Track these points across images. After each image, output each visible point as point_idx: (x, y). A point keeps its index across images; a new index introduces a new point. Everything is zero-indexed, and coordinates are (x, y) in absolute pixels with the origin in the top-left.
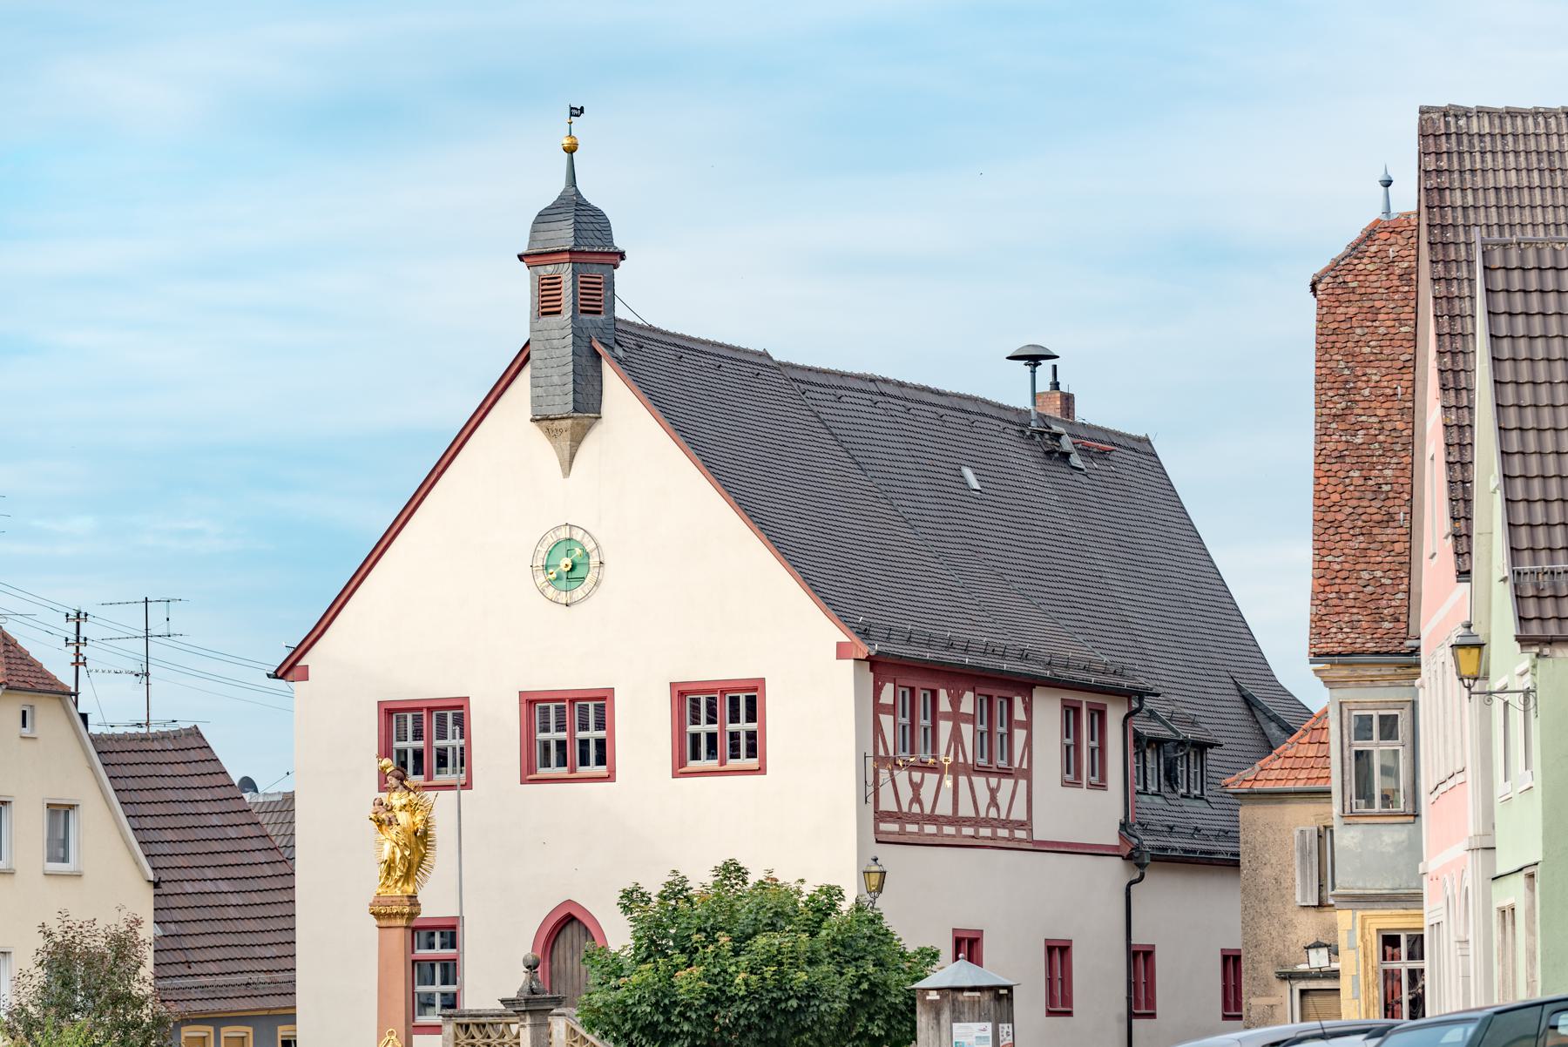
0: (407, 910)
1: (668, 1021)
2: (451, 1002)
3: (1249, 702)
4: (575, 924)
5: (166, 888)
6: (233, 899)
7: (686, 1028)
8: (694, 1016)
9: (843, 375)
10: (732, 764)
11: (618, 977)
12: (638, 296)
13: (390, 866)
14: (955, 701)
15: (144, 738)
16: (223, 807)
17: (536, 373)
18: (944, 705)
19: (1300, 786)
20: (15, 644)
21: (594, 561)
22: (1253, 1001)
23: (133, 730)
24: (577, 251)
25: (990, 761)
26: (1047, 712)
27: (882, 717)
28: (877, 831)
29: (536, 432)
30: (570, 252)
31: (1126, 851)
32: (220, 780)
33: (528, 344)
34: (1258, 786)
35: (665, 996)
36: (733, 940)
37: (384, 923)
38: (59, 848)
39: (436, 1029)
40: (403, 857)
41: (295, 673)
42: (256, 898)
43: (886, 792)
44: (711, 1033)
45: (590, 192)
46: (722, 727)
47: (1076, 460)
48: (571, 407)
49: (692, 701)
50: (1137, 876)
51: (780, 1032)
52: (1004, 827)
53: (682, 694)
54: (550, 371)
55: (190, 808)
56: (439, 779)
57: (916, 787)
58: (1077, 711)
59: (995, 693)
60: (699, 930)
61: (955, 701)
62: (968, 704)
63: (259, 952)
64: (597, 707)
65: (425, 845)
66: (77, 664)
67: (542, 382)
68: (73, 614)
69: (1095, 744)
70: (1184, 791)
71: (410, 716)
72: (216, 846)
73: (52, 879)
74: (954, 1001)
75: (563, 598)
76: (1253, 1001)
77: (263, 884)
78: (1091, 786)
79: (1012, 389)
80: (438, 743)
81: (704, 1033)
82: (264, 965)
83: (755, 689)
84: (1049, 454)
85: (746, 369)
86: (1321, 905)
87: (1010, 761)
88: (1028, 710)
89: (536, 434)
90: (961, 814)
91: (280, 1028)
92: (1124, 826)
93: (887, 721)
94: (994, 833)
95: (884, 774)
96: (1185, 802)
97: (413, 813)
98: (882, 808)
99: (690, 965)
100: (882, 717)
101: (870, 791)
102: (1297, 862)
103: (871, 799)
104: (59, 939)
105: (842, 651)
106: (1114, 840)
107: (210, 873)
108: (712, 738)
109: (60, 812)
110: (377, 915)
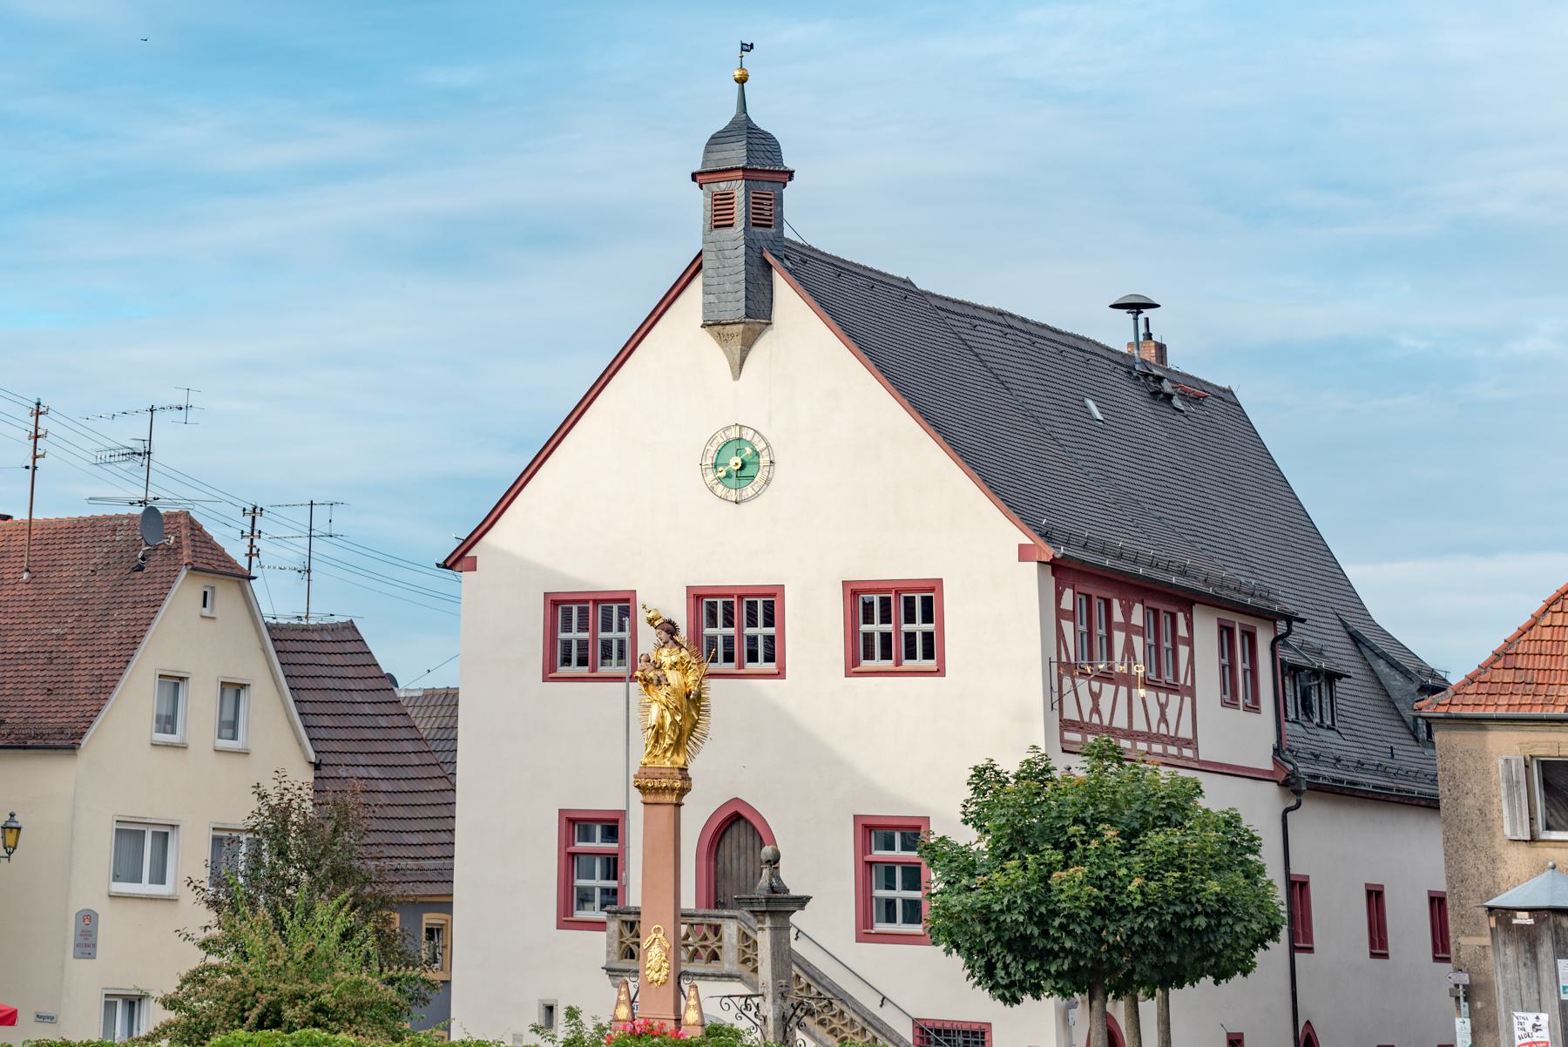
0: (678, 784)
1: (1045, 934)
2: (611, 896)
3: (1356, 639)
4: (742, 823)
5: (325, 772)
6: (384, 786)
7: (1068, 944)
8: (1079, 931)
9: (976, 307)
10: (908, 664)
11: (972, 876)
12: (804, 219)
13: (658, 733)
14: (1127, 613)
15: (305, 629)
16: (375, 697)
17: (709, 281)
18: (1118, 616)
19: (1502, 712)
20: (200, 529)
21: (764, 460)
22: (1463, 940)
23: (295, 622)
24: (750, 169)
25: (1159, 675)
26: (1206, 630)
27: (1063, 622)
28: (1062, 741)
29: (706, 338)
30: (744, 169)
31: (1282, 777)
32: (372, 671)
33: (700, 254)
34: (1454, 711)
35: (1040, 902)
36: (1121, 834)
37: (651, 799)
38: (230, 727)
39: (600, 926)
40: (674, 722)
41: (463, 563)
42: (405, 786)
43: (1069, 700)
44: (1097, 952)
45: (760, 120)
46: (897, 628)
47: (1177, 402)
48: (743, 312)
49: (867, 602)
50: (1293, 803)
51: (1181, 956)
52: (1173, 744)
53: (855, 593)
54: (721, 280)
55: (345, 696)
56: (603, 671)
57: (1096, 697)
58: (1231, 631)
59: (1162, 607)
60: (1076, 821)
61: (1127, 613)
62: (1137, 617)
63: (407, 838)
64: (765, 606)
65: (698, 711)
66: (250, 555)
67: (714, 289)
68: (249, 509)
69: (1247, 666)
70: (1317, 720)
71: (575, 609)
72: (369, 734)
73: (222, 756)
74: (1557, 927)
75: (733, 495)
76: (1463, 940)
77: (411, 773)
78: (1247, 708)
79: (1117, 334)
80: (603, 635)
81: (1090, 952)
82: (412, 852)
83: (932, 590)
84: (1154, 394)
85: (895, 292)
86: (1533, 840)
87: (1176, 677)
88: (1190, 627)
89: (707, 340)
90: (1136, 728)
91: (425, 916)
92: (1277, 751)
93: (1068, 626)
94: (1165, 750)
95: (1067, 682)
96: (1320, 731)
97: (685, 673)
98: (1066, 716)
99: (1066, 866)
100: (1063, 622)
101: (1055, 700)
102: (1503, 793)
103: (1056, 706)
104: (274, 802)
105: (1024, 553)
106: (1269, 766)
107: (362, 759)
108: (886, 637)
109: (234, 690)
110: (643, 789)
